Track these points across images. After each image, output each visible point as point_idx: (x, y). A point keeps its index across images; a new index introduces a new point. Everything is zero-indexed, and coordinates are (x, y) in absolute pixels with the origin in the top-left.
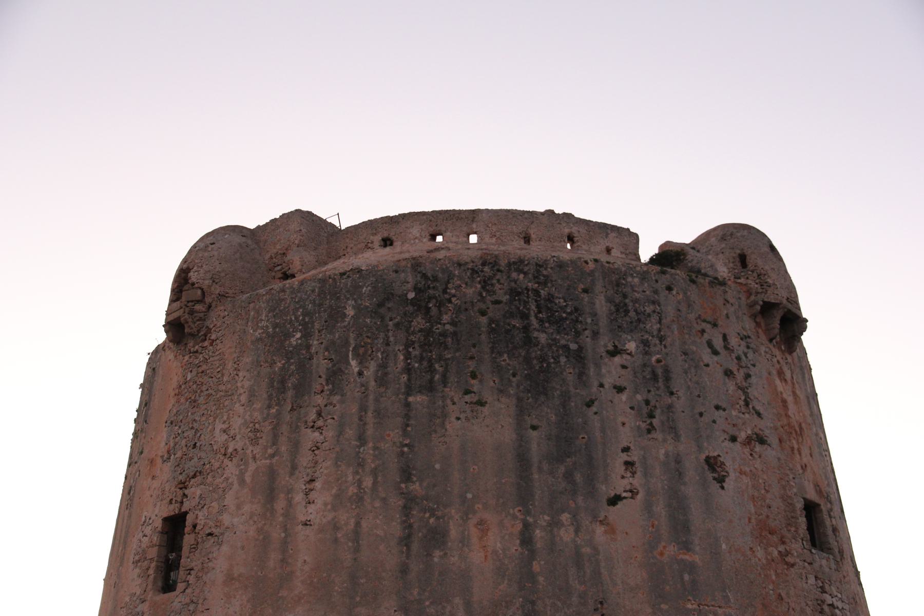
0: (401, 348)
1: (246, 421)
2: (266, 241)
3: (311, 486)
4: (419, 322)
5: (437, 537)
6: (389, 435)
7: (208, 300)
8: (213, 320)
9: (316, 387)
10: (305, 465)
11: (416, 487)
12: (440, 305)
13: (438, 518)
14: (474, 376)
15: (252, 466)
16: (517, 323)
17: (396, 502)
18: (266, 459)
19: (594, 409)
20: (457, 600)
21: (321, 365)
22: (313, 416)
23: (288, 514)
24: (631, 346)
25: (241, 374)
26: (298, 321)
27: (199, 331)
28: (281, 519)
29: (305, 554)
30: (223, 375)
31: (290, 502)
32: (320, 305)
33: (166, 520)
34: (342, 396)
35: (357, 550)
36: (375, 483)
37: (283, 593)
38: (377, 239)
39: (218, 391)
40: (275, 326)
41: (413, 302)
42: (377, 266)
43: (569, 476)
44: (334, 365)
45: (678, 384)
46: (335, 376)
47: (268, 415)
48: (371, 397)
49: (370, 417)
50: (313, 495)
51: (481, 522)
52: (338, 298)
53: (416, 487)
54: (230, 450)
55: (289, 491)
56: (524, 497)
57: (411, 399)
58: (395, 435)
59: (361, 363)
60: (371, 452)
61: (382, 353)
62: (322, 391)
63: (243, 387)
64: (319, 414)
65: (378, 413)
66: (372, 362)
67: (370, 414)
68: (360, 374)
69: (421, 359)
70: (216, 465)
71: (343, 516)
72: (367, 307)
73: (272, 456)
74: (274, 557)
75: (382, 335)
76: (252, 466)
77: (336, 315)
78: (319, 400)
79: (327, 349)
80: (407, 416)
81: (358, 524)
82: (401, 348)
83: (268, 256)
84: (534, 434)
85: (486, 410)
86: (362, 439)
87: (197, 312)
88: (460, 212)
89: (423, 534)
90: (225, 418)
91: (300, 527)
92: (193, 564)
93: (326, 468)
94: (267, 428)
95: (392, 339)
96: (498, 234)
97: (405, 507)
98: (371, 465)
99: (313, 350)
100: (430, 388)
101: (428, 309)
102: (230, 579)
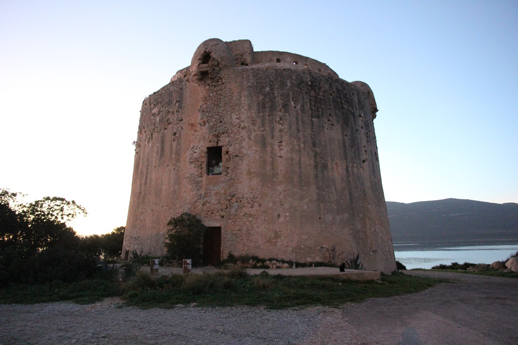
3: (281, 144)
4: (313, 93)
5: (325, 167)
7: (220, 66)
8: (222, 74)
9: (278, 109)
11: (317, 149)
12: (319, 89)
13: (325, 161)
14: (330, 115)
15: (254, 134)
16: (339, 100)
17: (312, 154)
19: (358, 133)
20: (333, 187)
21: (279, 101)
22: (278, 119)
23: (273, 152)
24: (362, 115)
25: (242, 98)
27: (215, 78)
28: (270, 154)
29: (281, 167)
30: (232, 97)
31: (273, 148)
33: (209, 148)
35: (300, 168)
36: (304, 146)
37: (275, 180)
38: (275, 59)
40: (257, 83)
41: (310, 86)
43: (355, 152)
46: (286, 106)
48: (300, 116)
50: (282, 147)
51: (336, 164)
52: (284, 78)
53: (317, 149)
54: (242, 126)
55: (272, 145)
56: (346, 158)
57: (313, 119)
58: (309, 131)
59: (295, 103)
63: (244, 103)
64: (281, 119)
65: (302, 122)
67: (300, 122)
68: (295, 107)
69: (315, 106)
70: (235, 131)
71: (295, 156)
73: (263, 131)
74: (268, 168)
75: (301, 95)
76: (254, 134)
77: (283, 85)
78: (280, 113)
79: (281, 96)
80: (312, 125)
81: (300, 159)
83: (233, 54)
84: (346, 138)
85: (334, 127)
86: (298, 130)
88: (303, 56)
89: (321, 166)
90: (237, 113)
91: (278, 158)
92: (229, 166)
97: (315, 156)
98: (302, 140)
99: (276, 95)
100: (318, 117)
101: (315, 90)
102: (249, 173)
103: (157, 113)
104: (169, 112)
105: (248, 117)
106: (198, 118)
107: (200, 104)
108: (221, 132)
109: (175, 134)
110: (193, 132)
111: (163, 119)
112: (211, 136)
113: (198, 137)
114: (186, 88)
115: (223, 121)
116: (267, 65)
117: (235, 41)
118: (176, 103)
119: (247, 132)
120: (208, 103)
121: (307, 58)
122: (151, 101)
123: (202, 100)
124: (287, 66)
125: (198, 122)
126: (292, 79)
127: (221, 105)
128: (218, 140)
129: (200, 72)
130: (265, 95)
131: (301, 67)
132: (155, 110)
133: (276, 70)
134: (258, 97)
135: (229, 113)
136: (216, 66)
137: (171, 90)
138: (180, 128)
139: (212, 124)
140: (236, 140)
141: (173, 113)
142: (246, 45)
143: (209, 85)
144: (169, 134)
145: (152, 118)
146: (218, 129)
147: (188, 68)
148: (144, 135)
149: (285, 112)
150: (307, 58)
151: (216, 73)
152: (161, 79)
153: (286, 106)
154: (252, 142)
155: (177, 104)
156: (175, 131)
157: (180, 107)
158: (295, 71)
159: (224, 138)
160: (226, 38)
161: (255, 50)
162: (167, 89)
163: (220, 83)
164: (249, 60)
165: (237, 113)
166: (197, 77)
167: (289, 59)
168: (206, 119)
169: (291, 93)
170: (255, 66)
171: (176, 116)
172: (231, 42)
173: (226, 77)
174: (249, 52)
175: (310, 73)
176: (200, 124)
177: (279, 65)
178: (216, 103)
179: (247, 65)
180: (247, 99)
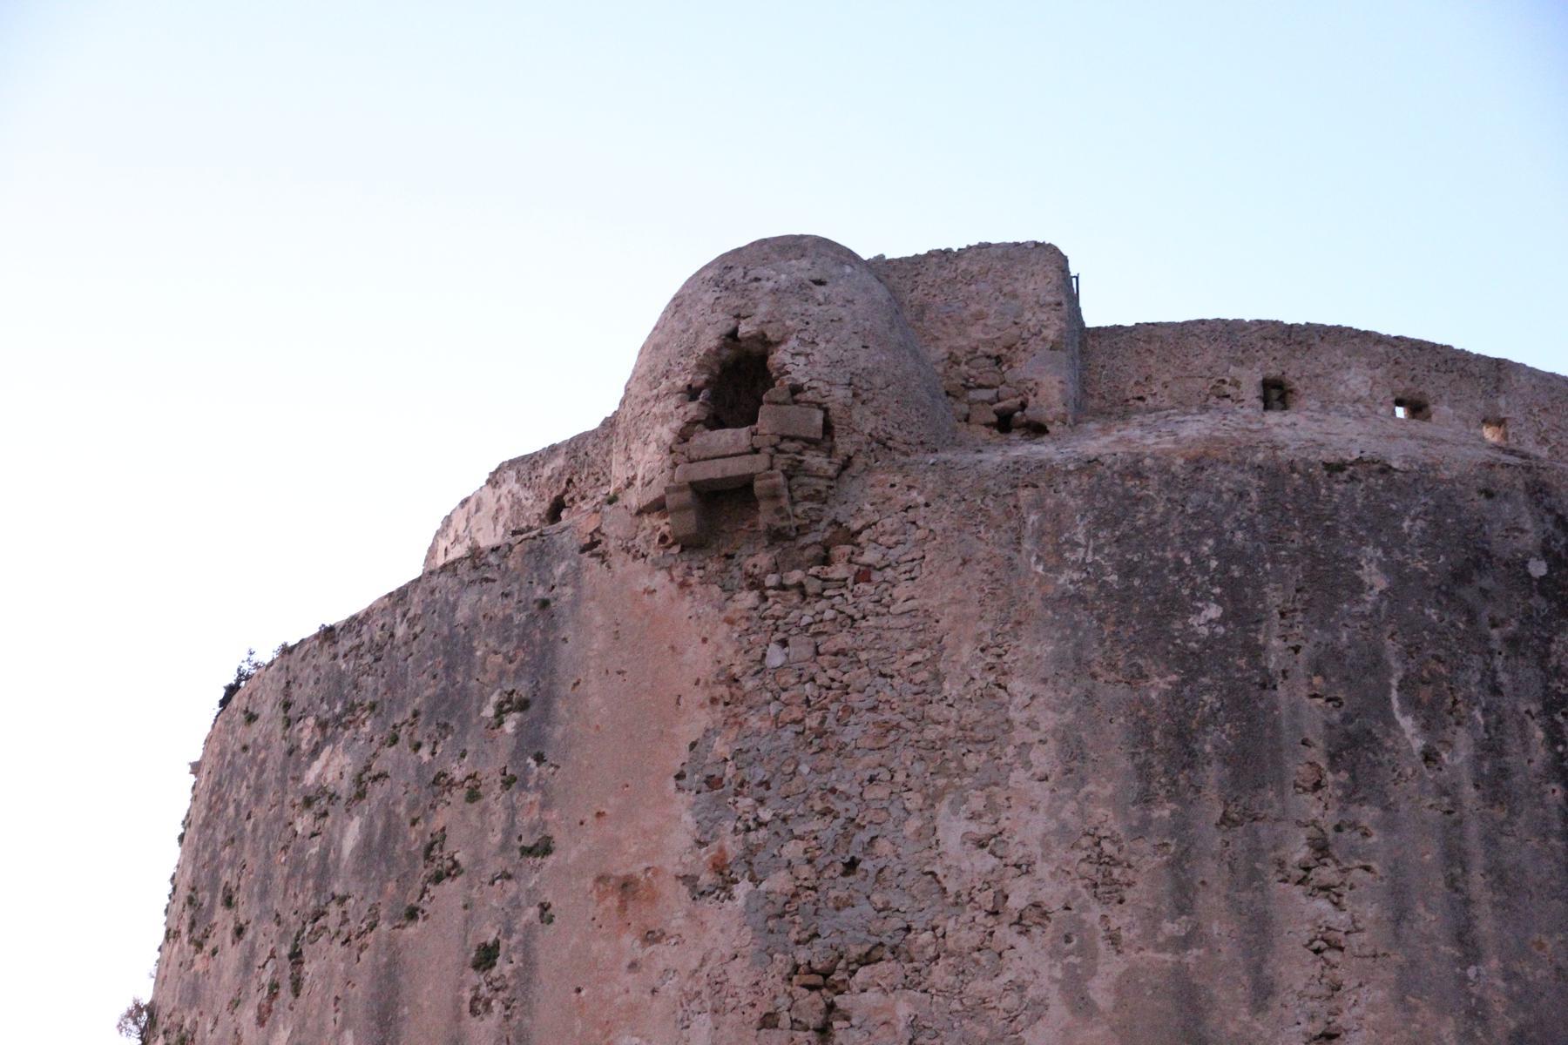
0: (1534, 708)
1: (1064, 825)
2: (923, 309)
6: (1541, 946)
7: (844, 445)
8: (861, 501)
9: (1297, 768)
10: (1299, 986)
15: (1110, 966)
18: (1160, 948)
21: (1303, 710)
22: (1300, 852)
25: (1015, 685)
26: (1206, 571)
27: (800, 530)
30: (938, 677)
32: (1274, 539)
34: (1386, 809)
39: (920, 721)
40: (1127, 570)
41: (1543, 586)
42: (1434, 467)
44: (1347, 719)
45: (468, 995)
46: (1355, 748)
47: (1146, 822)
48: (1474, 829)
49: (1477, 883)
52: (1330, 533)
54: (1017, 902)
60: (1500, 983)
61: (1485, 712)
62: (1317, 786)
63: (1032, 724)
64: (1321, 849)
65: (1499, 876)
66: (1461, 731)
68: (1429, 757)
72: (1424, 576)
73: (1184, 943)
75: (1476, 662)
76: (1110, 966)
77: (1328, 583)
78: (1311, 807)
79: (1317, 668)
82: (1534, 708)
83: (939, 352)
86: (1464, 938)
87: (808, 473)
88: (1464, 356)
90: (977, 803)
93: (1373, 1007)
94: (1147, 860)
95: (1503, 678)
96: (1553, 437)
103: (345, 787)
104: (441, 782)
105: (1063, 830)
106: (673, 833)
107: (696, 721)
108: (855, 951)
109: (486, 957)
110: (630, 941)
111: (391, 832)
112: (773, 981)
113: (670, 987)
114: (576, 603)
115: (867, 865)
116: (1195, 428)
117: (945, 255)
118: (500, 712)
119: (1055, 953)
120: (754, 721)
121: (1500, 367)
122: (299, 695)
123: (703, 695)
124: (1349, 436)
125: (672, 866)
126: (1400, 540)
127: (850, 734)
128: (831, 1007)
129: (695, 486)
130: (1191, 663)
131: (1460, 441)
132: (332, 767)
133: (1273, 475)
134: (1137, 676)
135: (914, 800)
136: (811, 443)
137: (462, 614)
138: (532, 912)
139: (779, 882)
140: (971, 1014)
141: (473, 796)
142: (1036, 286)
143: (755, 584)
144: (436, 952)
145: (303, 823)
146: (825, 925)
147: (582, 456)
148: (232, 955)
149: (1351, 795)
150: (1499, 371)
151: (815, 496)
152: (359, 532)
153: (1355, 748)
154: (1099, 1031)
155: (509, 726)
156: (490, 936)
157: (534, 746)
158: (1421, 479)
159: (872, 997)
160: (884, 229)
161: (1093, 317)
162: (428, 607)
163: (839, 571)
164: (1056, 396)
165: (977, 803)
166: (664, 525)
167: (1356, 380)
168: (733, 847)
169: (1391, 648)
170: (1096, 442)
171: (498, 818)
172: (917, 261)
173: (889, 523)
174: (1050, 334)
175: (1538, 491)
176: (689, 880)
177: (1294, 431)
178: (812, 721)
179: (1037, 430)
180: (1047, 694)
